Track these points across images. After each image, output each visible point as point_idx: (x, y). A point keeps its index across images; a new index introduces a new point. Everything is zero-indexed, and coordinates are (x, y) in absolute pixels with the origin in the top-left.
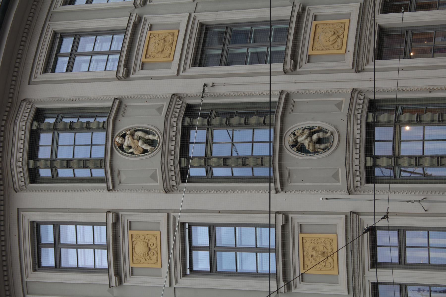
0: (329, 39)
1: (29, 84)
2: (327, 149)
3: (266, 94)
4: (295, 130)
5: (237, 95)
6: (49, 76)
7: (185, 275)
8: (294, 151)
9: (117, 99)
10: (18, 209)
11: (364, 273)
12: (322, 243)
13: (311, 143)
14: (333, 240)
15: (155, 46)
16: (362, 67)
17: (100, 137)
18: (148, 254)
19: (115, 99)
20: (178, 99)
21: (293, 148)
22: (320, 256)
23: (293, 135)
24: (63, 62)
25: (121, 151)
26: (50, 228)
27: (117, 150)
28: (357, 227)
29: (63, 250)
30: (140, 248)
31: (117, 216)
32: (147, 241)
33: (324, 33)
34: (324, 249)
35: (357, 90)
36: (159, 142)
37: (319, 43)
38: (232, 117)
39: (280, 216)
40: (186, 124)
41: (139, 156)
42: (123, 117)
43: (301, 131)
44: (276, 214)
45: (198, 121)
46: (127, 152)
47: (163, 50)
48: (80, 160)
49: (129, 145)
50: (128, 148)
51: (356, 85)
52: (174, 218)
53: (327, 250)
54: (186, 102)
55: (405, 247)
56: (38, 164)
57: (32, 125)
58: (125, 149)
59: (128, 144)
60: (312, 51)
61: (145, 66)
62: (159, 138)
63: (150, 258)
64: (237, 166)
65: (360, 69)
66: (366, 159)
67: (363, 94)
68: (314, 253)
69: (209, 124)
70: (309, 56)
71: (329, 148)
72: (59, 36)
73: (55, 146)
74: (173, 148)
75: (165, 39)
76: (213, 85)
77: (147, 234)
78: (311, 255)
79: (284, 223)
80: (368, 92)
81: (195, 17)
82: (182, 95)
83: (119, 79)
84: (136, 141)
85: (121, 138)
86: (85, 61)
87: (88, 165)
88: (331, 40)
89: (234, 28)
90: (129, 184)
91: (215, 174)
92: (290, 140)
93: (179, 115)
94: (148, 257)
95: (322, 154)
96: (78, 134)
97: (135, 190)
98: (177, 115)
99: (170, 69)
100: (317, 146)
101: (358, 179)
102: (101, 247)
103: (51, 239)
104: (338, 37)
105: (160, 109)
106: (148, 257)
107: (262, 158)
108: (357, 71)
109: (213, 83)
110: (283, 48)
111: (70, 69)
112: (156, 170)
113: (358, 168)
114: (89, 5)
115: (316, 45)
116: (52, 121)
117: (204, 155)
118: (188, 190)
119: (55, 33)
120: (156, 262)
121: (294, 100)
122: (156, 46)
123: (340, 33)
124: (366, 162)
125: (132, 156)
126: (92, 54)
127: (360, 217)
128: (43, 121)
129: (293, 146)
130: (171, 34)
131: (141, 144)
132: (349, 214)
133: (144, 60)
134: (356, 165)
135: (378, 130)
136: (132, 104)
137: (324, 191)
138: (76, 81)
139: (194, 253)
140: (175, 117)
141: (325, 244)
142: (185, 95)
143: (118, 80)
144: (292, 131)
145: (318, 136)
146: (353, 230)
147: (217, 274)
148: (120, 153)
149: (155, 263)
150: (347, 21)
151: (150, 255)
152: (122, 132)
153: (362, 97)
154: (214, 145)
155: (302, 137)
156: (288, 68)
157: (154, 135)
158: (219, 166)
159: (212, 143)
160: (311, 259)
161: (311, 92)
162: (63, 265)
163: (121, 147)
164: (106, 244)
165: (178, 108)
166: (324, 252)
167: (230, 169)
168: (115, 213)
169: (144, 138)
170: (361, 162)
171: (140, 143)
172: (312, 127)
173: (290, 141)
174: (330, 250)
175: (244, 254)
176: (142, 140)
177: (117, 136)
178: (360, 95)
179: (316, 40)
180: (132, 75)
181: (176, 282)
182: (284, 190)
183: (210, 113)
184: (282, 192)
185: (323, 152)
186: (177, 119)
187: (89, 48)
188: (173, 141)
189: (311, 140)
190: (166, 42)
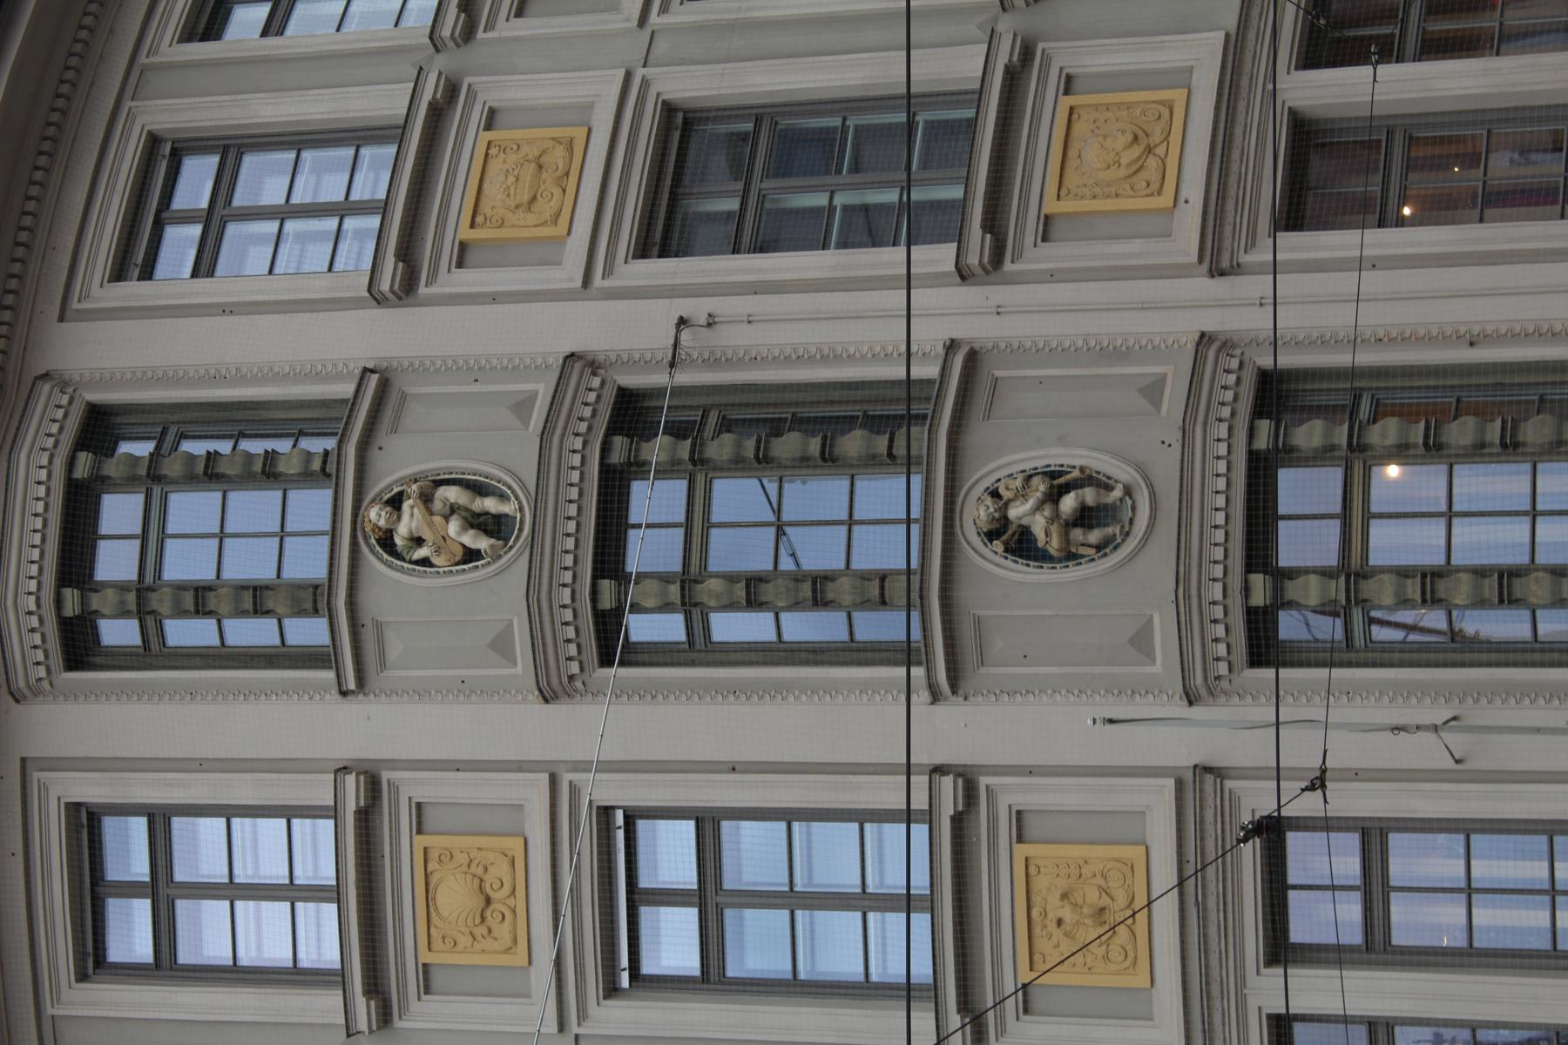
1: (61, 319)
2: (1111, 547)
4: (999, 480)
5: (794, 356)
6: (133, 291)
7: (611, 990)
8: (996, 553)
9: (372, 371)
10: (23, 760)
11: (1241, 982)
12: (1095, 875)
13: (1056, 525)
14: (1132, 867)
17: (312, 506)
18: (483, 919)
19: (365, 370)
20: (588, 370)
22: (1088, 921)
23: (992, 497)
24: (181, 242)
25: (386, 556)
26: (139, 825)
27: (372, 551)
28: (1216, 821)
29: (181, 905)
30: (454, 897)
31: (373, 786)
32: (480, 871)
33: (1100, 139)
36: (522, 522)
37: (1083, 174)
39: (947, 783)
40: (616, 458)
41: (452, 571)
43: (1018, 483)
45: (657, 449)
46: (407, 558)
47: (534, 198)
48: (242, 587)
49: (416, 535)
50: (409, 544)
51: (1211, 322)
52: (574, 790)
53: (1113, 900)
54: (615, 381)
55: (1387, 889)
56: (95, 602)
57: (71, 464)
58: (399, 549)
59: (411, 532)
61: (471, 256)
62: (521, 509)
63: (490, 931)
64: (796, 606)
65: (1225, 264)
66: (1246, 581)
67: (1238, 352)
68: (1067, 914)
69: (698, 460)
70: (1047, 217)
71: (1119, 540)
72: (167, 149)
73: (153, 537)
74: (570, 543)
77: (479, 849)
78: (1055, 921)
79: (960, 808)
81: (645, 83)
82: (601, 358)
83: (378, 303)
84: (438, 519)
85: (388, 509)
86: (259, 239)
87: (270, 604)
88: (1124, 161)
89: (784, 122)
90: (416, 673)
91: (717, 636)
92: (982, 513)
93: (590, 428)
94: (483, 930)
95: (1093, 564)
96: (232, 496)
99: (560, 264)
100: (1077, 534)
101: (1221, 649)
102: (315, 893)
103: (139, 868)
104: (1149, 152)
105: (522, 407)
106: (483, 930)
108: (1217, 272)
109: (710, 315)
110: (956, 192)
111: (205, 265)
112: (511, 622)
113: (1218, 612)
114: (272, 41)
115: (1072, 180)
116: (143, 449)
118: (624, 692)
119: (154, 141)
121: (993, 375)
122: (509, 184)
123: (1157, 137)
124: (1247, 590)
125: (426, 572)
126: (284, 213)
127: (1229, 784)
128: (111, 452)
129: (991, 535)
131: (457, 529)
132: (1189, 776)
133: (466, 233)
134: (1214, 603)
135: (1287, 479)
136: (425, 390)
138: (227, 310)
139: (645, 912)
140: (577, 435)
141: (1106, 878)
142: (613, 358)
143: (375, 303)
145: (1080, 499)
147: (726, 987)
148: (385, 563)
149: (508, 950)
150: (1178, 95)
152: (389, 487)
153: (1234, 364)
154: (713, 531)
155: (1023, 504)
156: (973, 260)
157: (502, 497)
158: (731, 606)
160: (1058, 934)
162: (184, 957)
163: (386, 541)
164: (335, 883)
165: (586, 404)
166: (1103, 909)
167: (770, 616)
168: (366, 772)
169: (467, 510)
170: (1230, 592)
171: (453, 527)
172: (1057, 468)
174: (1122, 900)
175: (820, 915)
176: (459, 514)
177: (373, 501)
178: (1228, 355)
179: (1072, 163)
181: (582, 1016)
182: (961, 691)
184: (954, 698)
186: (585, 443)
187: (272, 193)
189: (1056, 515)
190: (544, 170)
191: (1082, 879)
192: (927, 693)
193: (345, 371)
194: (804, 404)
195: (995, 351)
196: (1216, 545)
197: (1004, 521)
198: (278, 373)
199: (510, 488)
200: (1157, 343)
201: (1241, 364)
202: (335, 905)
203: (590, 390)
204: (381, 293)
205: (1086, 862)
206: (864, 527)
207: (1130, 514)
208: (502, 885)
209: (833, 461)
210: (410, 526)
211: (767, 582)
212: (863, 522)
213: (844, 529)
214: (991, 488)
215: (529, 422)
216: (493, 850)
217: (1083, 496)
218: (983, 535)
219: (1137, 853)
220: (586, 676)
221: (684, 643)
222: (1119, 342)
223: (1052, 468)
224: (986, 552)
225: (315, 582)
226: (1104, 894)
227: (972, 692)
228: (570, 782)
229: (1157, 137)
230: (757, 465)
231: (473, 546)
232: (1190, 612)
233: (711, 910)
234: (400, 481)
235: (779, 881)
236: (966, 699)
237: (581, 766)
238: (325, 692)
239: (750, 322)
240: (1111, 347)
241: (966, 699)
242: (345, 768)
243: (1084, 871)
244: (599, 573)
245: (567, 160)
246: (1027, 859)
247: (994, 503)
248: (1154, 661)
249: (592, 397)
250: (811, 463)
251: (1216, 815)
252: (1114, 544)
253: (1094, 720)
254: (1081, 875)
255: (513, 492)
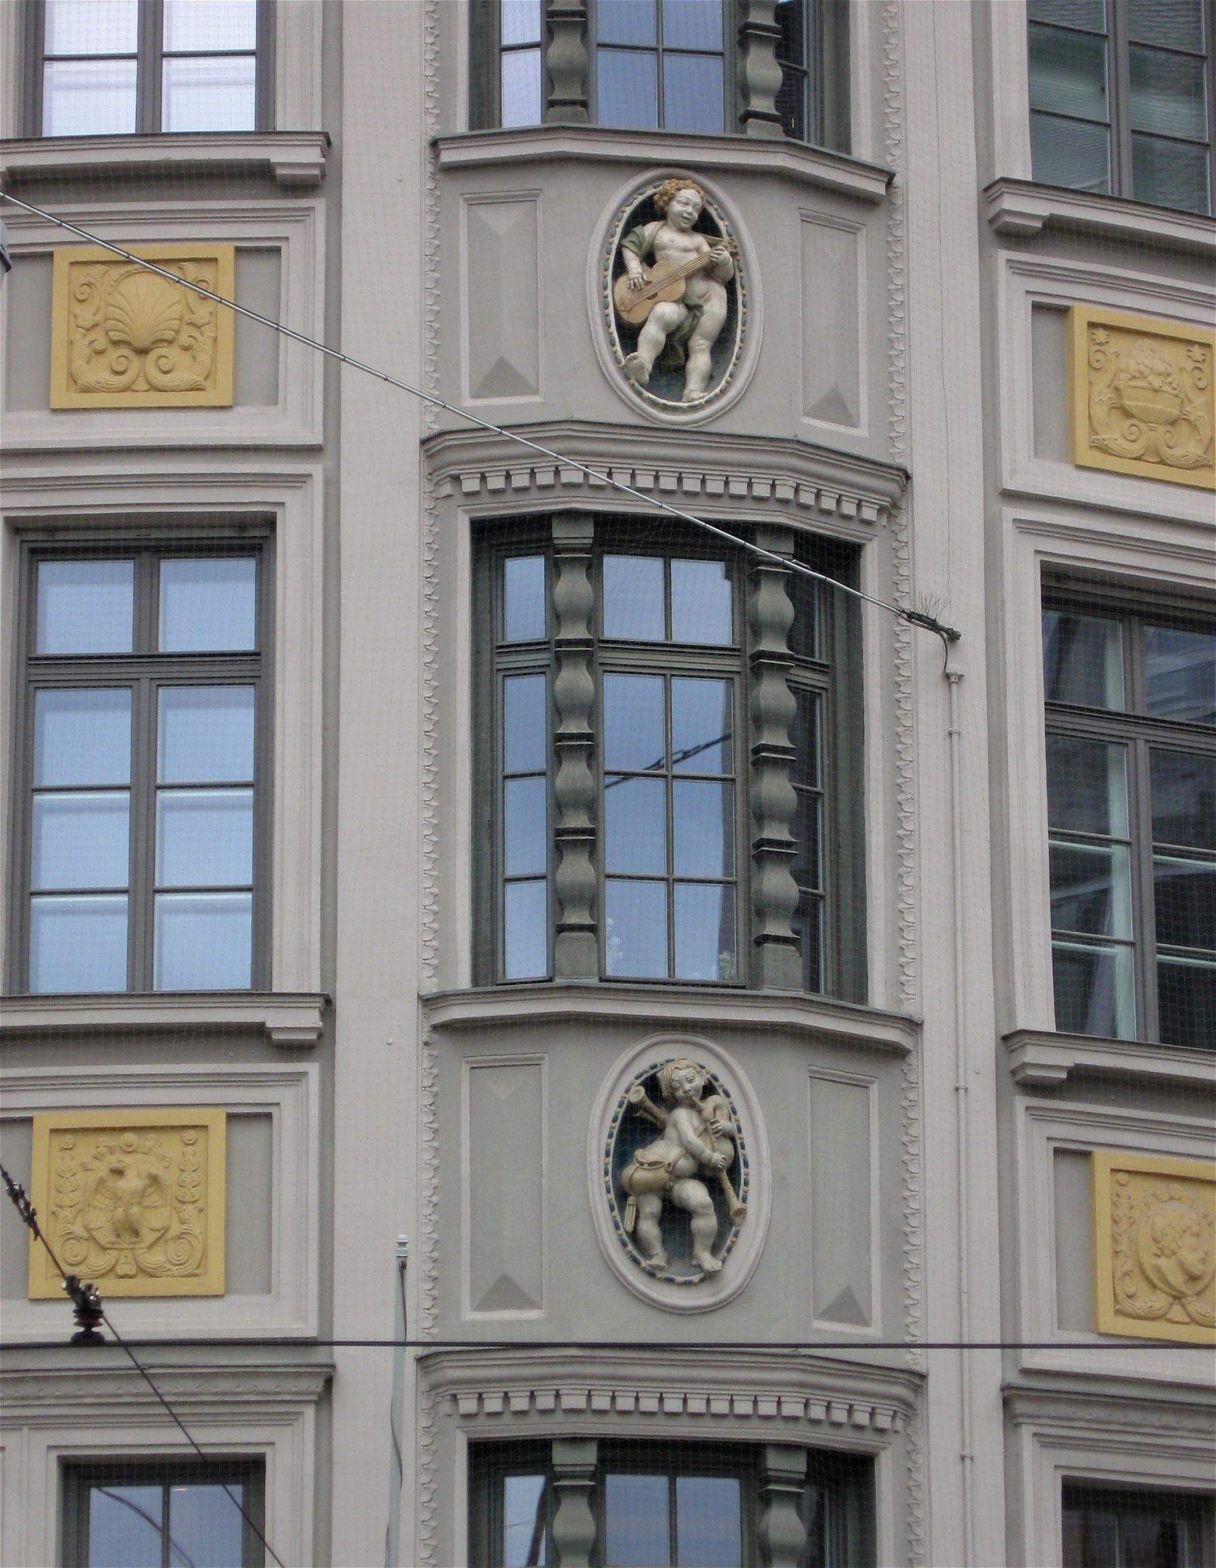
0: (1168, 1252)
2: (635, 1253)
3: (902, 942)
4: (727, 1095)
5: (901, 797)
8: (627, 1091)
9: (889, 184)
11: (39, 1424)
12: (183, 1222)
13: (666, 1175)
14: (196, 1275)
15: (1147, 372)
16: (1029, 1416)
18: (116, 343)
19: (890, 176)
20: (886, 502)
21: (644, 1084)
22: (120, 1212)
23: (704, 1087)
25: (629, 210)
27: (638, 189)
28: (258, 1393)
32: (184, 339)
33: (1195, 1228)
34: (153, 1230)
35: (916, 1396)
36: (675, 410)
37: (1147, 1205)
38: (778, 56)
39: (311, 1018)
41: (607, 308)
42: (799, 218)
43: (724, 1124)
44: (321, 1000)
46: (625, 242)
47: (1127, 414)
49: (658, 255)
50: (645, 245)
52: (298, 481)
53: (151, 1247)
54: (870, 540)
58: (638, 229)
59: (663, 248)
60: (1112, 1170)
61: (1049, 325)
62: (694, 409)
63: (100, 353)
65: (1020, 1407)
66: (591, 1439)
67: (899, 1425)
68: (132, 1182)
69: (760, 665)
70: (1086, 1155)
71: (644, 1263)
75: (1183, 422)
76: (953, 679)
77: (215, 340)
78: (120, 1166)
79: (276, 1036)
80: (909, 1447)
82: (903, 520)
83: (987, 189)
84: (681, 287)
85: (696, 215)
88: (1163, 1262)
90: (464, 269)
92: (683, 1073)
93: (805, 507)
94: (101, 343)
95: (611, 1226)
97: (437, 280)
98: (807, 498)
99: (1036, 456)
100: (653, 1205)
101: (494, 1405)
104: (1174, 1297)
106: (101, 343)
107: (592, 929)
108: (1009, 1397)
109: (961, 677)
110: (1126, 1029)
112: (535, 392)
113: (545, 1402)
115: (1139, 1190)
117: (611, 632)
120: (80, 382)
121: (872, 1082)
122: (1151, 378)
124: (576, 1441)
125: (606, 270)
127: (309, 1412)
129: (652, 1084)
130: (1205, 453)
131: (667, 317)
133: (1082, 315)
134: (558, 1396)
135: (726, 1490)
136: (862, 260)
137: (435, 1236)
140: (797, 490)
141: (180, 1238)
142: (903, 537)
143: (985, 185)
144: (725, 1080)
145: (700, 1210)
146: (245, 1374)
147: (22, 691)
148: (619, 210)
149: (72, 378)
151: (114, 354)
152: (726, 215)
153: (883, 1421)
154: (659, 682)
155: (695, 1129)
157: (711, 379)
159: (668, 673)
160: (102, 1170)
161: (913, 1169)
163: (649, 211)
164: (164, 130)
165: (839, 501)
166: (136, 1233)
168: (323, 176)
169: (692, 330)
170: (574, 1418)
171: (669, 311)
172: (743, 1177)
173: (676, 1071)
174: (154, 1259)
176: (687, 318)
177: (707, 191)
178: (895, 1412)
179: (1161, 1187)
180: (1008, 261)
182: (436, 1037)
183: (817, 660)
184: (427, 1028)
185: (622, 1231)
186: (784, 502)
188: (680, 480)
189: (677, 1176)
190: (1169, 428)
191: (177, 1204)
192: (435, 990)
193: (889, 142)
194: (835, 809)
195: (904, 1085)
196: (637, 1399)
197: (672, 1103)
198: (887, 43)
199: (723, 392)
200: (912, 1312)
201: (881, 1431)
202: (133, 131)
203: (859, 506)
204: (1001, 195)
205: (201, 1210)
206: (661, 800)
207: (680, 1279)
208: (165, 373)
209: (755, 763)
210: (671, 248)
211: (589, 766)
212: (670, 895)
213: (662, 873)
214: (716, 1084)
215: (815, 417)
216: (214, 360)
217: (704, 1215)
218: (652, 1072)
219: (214, 1280)
220: (459, 500)
221: (503, 639)
222: (915, 1260)
223: (743, 1170)
224: (629, 1077)
225: (591, 103)
226: (156, 1235)
227: (435, 1053)
228: (310, 476)
229: (1197, 1306)
230: (751, 747)
231: (642, 339)
232: (546, 1364)
233: (133, 671)
234: (734, 233)
235: (170, 769)
236: (426, 1044)
237: (333, 485)
238: (437, 116)
239: (950, 734)
240: (908, 1247)
241: (426, 1044)
242: (329, 143)
243: (190, 1207)
244: (602, 521)
245: (1183, 462)
246: (205, 1127)
247: (696, 1090)
248: (478, 1308)
249: (849, 509)
250: (740, 100)
251: (268, 1393)
252: (639, 1257)
253: (403, 1244)
254: (184, 1203)
255: (717, 397)
